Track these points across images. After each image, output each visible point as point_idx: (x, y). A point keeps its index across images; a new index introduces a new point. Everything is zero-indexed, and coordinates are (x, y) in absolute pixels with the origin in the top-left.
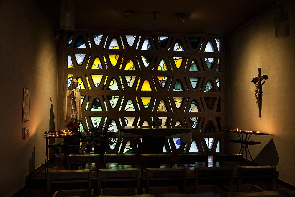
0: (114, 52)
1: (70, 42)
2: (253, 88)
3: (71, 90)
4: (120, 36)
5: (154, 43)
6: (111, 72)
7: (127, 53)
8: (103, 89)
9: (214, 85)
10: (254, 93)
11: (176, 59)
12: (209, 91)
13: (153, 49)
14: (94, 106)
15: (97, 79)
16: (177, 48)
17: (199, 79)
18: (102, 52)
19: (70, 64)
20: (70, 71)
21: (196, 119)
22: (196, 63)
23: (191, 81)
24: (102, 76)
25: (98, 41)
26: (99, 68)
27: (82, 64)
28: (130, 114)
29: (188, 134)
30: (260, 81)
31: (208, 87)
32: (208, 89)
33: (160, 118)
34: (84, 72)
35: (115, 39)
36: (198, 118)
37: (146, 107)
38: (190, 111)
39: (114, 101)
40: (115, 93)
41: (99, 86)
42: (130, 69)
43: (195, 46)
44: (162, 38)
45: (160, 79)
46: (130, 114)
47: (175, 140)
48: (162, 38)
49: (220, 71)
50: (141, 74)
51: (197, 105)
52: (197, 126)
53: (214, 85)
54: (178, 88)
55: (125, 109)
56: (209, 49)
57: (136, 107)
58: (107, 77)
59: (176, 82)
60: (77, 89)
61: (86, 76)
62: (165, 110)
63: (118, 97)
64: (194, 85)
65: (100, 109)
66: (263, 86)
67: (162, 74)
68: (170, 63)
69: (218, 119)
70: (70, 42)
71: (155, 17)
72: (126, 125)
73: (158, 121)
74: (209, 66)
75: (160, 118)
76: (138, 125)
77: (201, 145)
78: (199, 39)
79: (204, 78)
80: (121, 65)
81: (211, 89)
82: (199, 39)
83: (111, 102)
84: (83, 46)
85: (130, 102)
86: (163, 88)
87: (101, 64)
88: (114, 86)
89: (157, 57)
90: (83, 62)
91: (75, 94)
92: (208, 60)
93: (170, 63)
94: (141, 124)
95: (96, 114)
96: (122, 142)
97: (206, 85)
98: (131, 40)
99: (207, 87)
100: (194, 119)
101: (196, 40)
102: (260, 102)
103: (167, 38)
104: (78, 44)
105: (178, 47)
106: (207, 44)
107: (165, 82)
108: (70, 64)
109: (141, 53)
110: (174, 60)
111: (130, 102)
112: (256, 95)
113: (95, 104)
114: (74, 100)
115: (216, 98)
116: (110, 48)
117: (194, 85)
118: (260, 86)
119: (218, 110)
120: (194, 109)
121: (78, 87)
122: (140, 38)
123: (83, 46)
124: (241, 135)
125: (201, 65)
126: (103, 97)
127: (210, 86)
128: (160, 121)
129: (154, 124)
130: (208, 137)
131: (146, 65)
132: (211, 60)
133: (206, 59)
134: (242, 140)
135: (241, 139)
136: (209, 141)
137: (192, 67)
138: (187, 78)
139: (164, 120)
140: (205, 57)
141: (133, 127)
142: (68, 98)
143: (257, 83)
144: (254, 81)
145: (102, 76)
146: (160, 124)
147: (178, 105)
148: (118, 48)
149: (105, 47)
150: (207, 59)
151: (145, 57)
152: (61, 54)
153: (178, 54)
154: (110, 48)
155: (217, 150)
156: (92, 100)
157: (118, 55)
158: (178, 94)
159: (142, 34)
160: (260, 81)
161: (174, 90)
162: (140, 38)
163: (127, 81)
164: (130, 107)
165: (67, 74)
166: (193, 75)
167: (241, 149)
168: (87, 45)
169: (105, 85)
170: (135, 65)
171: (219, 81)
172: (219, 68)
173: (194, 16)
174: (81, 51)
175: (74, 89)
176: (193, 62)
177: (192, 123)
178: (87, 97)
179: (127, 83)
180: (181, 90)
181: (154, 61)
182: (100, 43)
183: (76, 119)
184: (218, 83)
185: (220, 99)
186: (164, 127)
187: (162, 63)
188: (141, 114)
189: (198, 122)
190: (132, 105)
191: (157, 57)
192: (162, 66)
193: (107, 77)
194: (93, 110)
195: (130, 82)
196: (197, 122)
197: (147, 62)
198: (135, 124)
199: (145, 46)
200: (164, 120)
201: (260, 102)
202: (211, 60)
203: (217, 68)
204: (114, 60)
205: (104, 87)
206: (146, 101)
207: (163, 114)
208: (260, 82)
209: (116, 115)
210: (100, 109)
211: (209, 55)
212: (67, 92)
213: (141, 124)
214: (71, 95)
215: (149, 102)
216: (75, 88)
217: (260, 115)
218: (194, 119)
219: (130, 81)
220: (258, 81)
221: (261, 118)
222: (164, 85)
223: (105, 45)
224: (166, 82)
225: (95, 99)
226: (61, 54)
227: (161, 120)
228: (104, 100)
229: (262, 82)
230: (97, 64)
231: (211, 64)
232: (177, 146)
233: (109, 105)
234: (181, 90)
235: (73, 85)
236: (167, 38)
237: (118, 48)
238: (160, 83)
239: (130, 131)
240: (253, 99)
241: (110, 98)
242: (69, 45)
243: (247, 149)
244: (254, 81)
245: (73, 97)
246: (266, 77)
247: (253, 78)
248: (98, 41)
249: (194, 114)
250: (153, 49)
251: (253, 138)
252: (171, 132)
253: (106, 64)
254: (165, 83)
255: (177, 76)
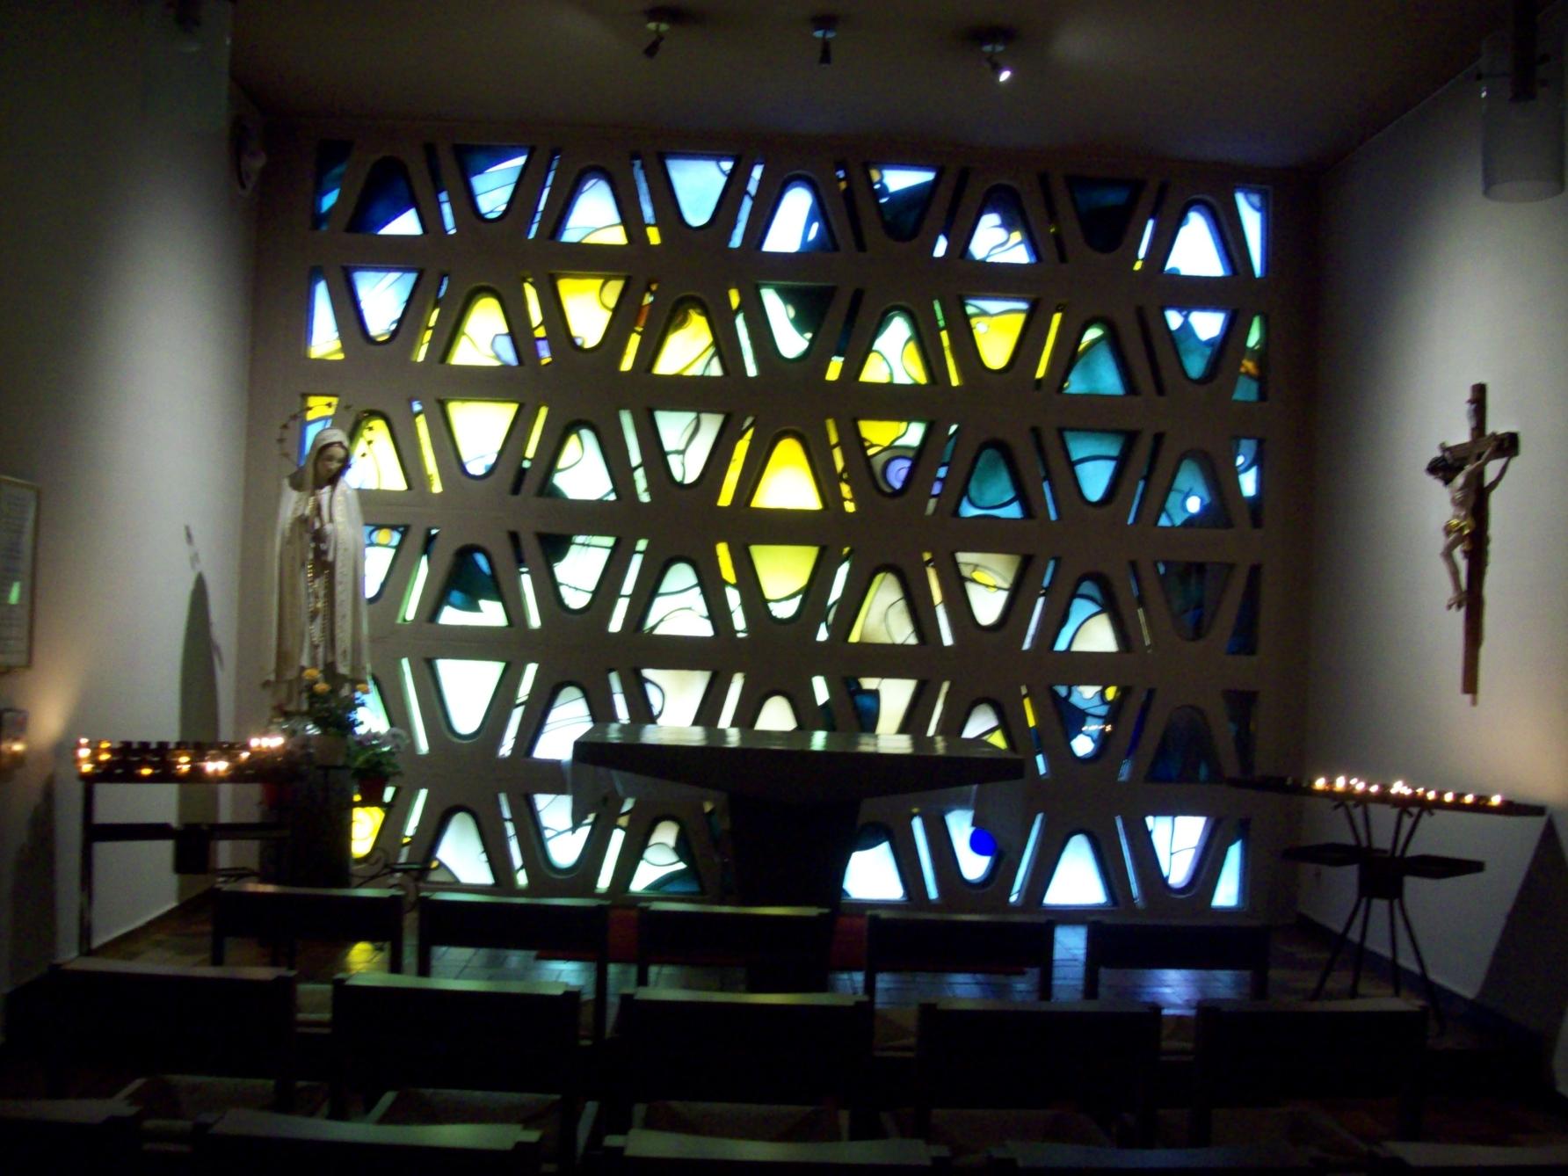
0: (591, 260)
1: (329, 201)
2: (1439, 506)
3: (304, 495)
4: (635, 162)
5: (845, 210)
6: (574, 389)
7: (677, 272)
8: (516, 489)
9: (1220, 482)
10: (1441, 542)
11: (984, 313)
12: (1191, 522)
13: (836, 248)
14: (456, 596)
15: (481, 430)
16: (995, 241)
17: (1130, 440)
18: (523, 256)
19: (325, 340)
20: (324, 377)
21: (1102, 694)
22: (1113, 339)
23: (1075, 456)
24: (511, 409)
25: (494, 189)
26: (498, 357)
27: (394, 334)
28: (679, 653)
29: (1028, 796)
30: (1470, 467)
31: (1187, 495)
32: (1184, 509)
33: (869, 683)
34: (403, 382)
35: (600, 178)
36: (1111, 693)
37: (784, 610)
38: (1061, 645)
39: (580, 570)
40: (590, 517)
41: (491, 471)
42: (688, 373)
43: (1111, 233)
44: (898, 180)
45: (878, 433)
46: (679, 653)
47: (960, 826)
48: (898, 180)
49: (1263, 395)
50: (759, 404)
51: (1110, 606)
52: (1103, 741)
53: (1220, 482)
54: (994, 498)
55: (650, 622)
56: (1195, 251)
57: (717, 612)
58: (543, 412)
59: (976, 460)
60: (341, 486)
61: (417, 407)
62: (902, 632)
63: (610, 541)
64: (1095, 480)
65: (491, 614)
66: (1495, 500)
67: (893, 402)
68: (944, 334)
69: (1242, 703)
70: (329, 201)
71: (826, 57)
72: (652, 719)
73: (855, 707)
74: (1195, 366)
75: (869, 683)
76: (931, 731)
77: (1123, 858)
78: (1135, 187)
79: (1159, 438)
80: (634, 341)
81: (1205, 509)
82: (1135, 187)
83: (562, 570)
84: (407, 224)
85: (681, 576)
86: (896, 493)
87: (512, 334)
88: (583, 473)
89: (858, 297)
90: (400, 322)
91: (331, 520)
92: (1186, 326)
93: (944, 334)
94: (746, 715)
95: (473, 644)
96: (623, 821)
97: (1174, 477)
98: (698, 186)
99: (1173, 499)
100: (1086, 695)
101: (1114, 198)
102: (1472, 601)
103: (926, 177)
104: (379, 210)
105: (1001, 234)
106: (1180, 220)
107: (911, 454)
108: (325, 340)
109: (759, 267)
110: (967, 318)
111: (681, 576)
112: (1448, 554)
113: (462, 579)
114: (320, 554)
115: (1231, 567)
116: (570, 235)
117: (1095, 480)
118: (1476, 502)
119: (1245, 641)
120: (1094, 634)
121: (359, 476)
122: (757, 172)
123: (407, 224)
124: (1358, 813)
125: (1145, 350)
126: (514, 537)
127: (1199, 486)
128: (866, 702)
129: (825, 717)
130: (1171, 809)
131: (791, 342)
132: (1208, 325)
133: (1174, 319)
134: (1364, 843)
135: (1357, 838)
136: (1177, 841)
137: (1087, 365)
138: (1050, 439)
139: (894, 695)
140: (1172, 307)
141: (696, 737)
142: (288, 542)
143: (1460, 480)
144: (1444, 468)
145: (511, 409)
146: (868, 720)
147: (987, 605)
148: (618, 237)
149: (535, 228)
150: (1186, 317)
151: (787, 295)
152: (276, 260)
153: (998, 280)
154: (570, 235)
155: (1227, 893)
156: (445, 552)
157: (616, 278)
158: (988, 536)
159: (766, 154)
160: (1470, 467)
161: (969, 511)
162: (757, 172)
163: (667, 447)
164: (680, 610)
165: (305, 396)
166: (1094, 415)
167: (1359, 901)
168: (430, 220)
169: (526, 464)
170: (725, 346)
171: (1258, 460)
172: (1261, 379)
173: (1079, 45)
174: (394, 255)
175: (327, 489)
176: (1093, 333)
177: (1074, 719)
178: (417, 539)
179: (664, 455)
180: (1013, 511)
181: (841, 318)
182: (510, 203)
183: (330, 671)
184: (1247, 469)
185: (1255, 570)
186: (889, 738)
187: (897, 332)
188: (758, 653)
189: (1114, 713)
190: (696, 599)
191: (858, 297)
192: (894, 357)
193: (543, 412)
194: (451, 616)
195: (682, 452)
196: (1106, 719)
197: (801, 323)
198: (707, 713)
199: (792, 224)
200: (894, 695)
201: (1472, 601)
202: (1208, 325)
203: (1248, 374)
204: (588, 308)
205: (522, 477)
206: (784, 572)
207: (888, 660)
208: (1479, 474)
209: (595, 654)
210: (491, 614)
211: (1196, 293)
212: (284, 500)
213: (746, 715)
214: (302, 521)
215: (802, 580)
216: (333, 479)
217: (1470, 683)
218: (1086, 695)
219: (687, 441)
220: (1468, 468)
221: (1474, 702)
222: (903, 474)
223: (538, 218)
224: (920, 457)
225: (465, 554)
226: (276, 260)
227: (875, 694)
228: (520, 561)
229: (1492, 470)
230: (483, 337)
231: (1208, 351)
232: (974, 866)
233: (549, 591)
234: (1013, 511)
235: (320, 465)
236: (926, 177)
237: (618, 237)
238: (878, 464)
239: (671, 759)
240: (1434, 582)
241: (556, 546)
242: (318, 219)
243: (1396, 902)
244: (1444, 468)
245: (319, 537)
246: (1508, 445)
247: (1444, 448)
248: (494, 189)
249: (1090, 667)
250: (836, 248)
251: (1432, 838)
252: (933, 776)
253: (541, 333)
254: (907, 464)
255: (992, 423)
